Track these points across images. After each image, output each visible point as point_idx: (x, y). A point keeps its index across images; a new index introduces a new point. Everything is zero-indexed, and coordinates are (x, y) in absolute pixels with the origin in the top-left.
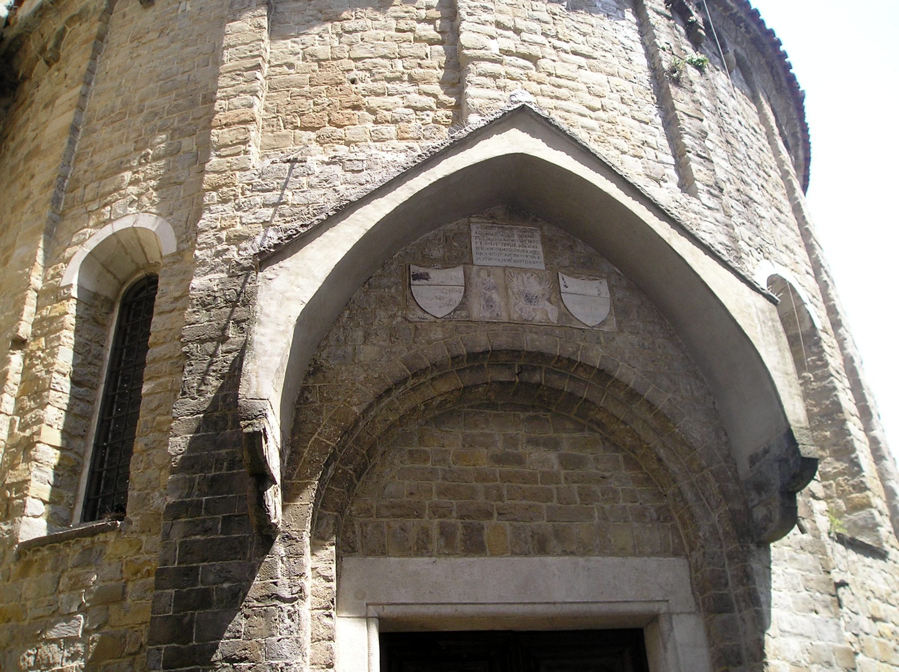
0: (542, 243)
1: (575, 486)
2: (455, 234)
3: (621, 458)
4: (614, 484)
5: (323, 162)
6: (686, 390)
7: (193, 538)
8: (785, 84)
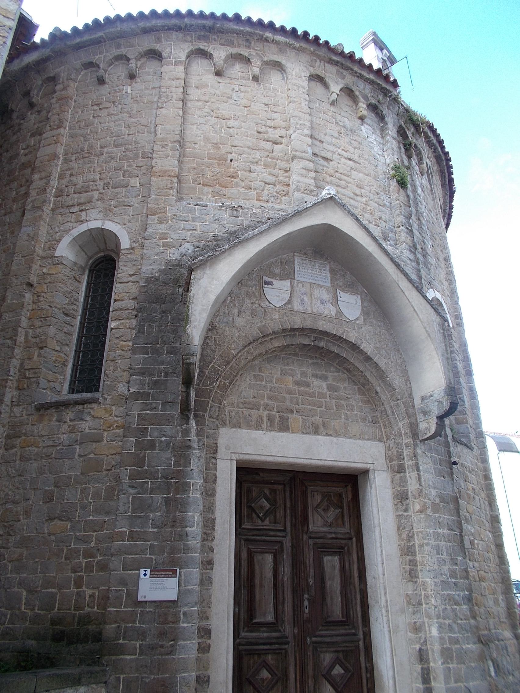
0: (330, 272)
1: (334, 401)
2: (287, 261)
3: (356, 389)
4: (352, 402)
7: (145, 412)
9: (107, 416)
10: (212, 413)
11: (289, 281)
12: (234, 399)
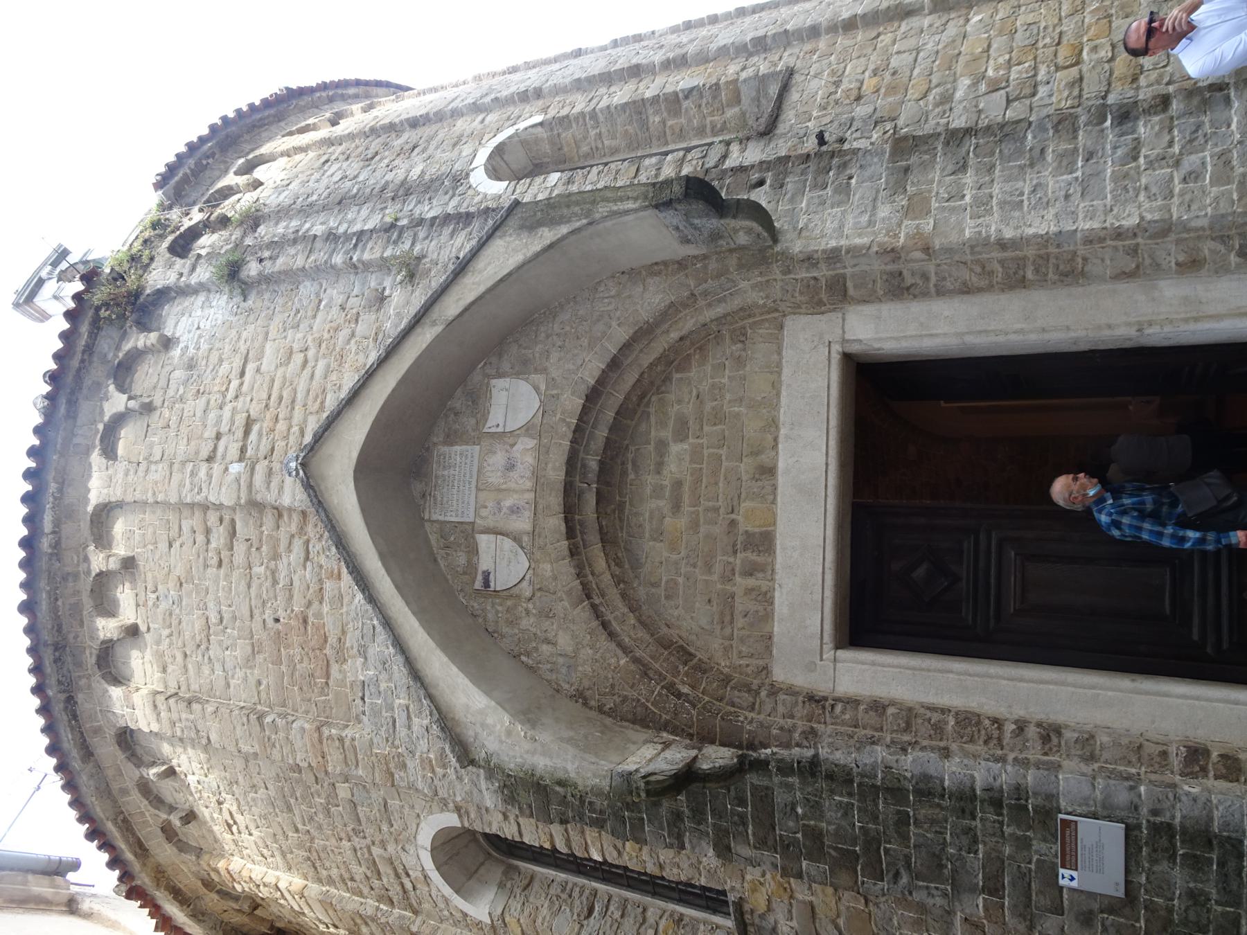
1: (706, 428)
4: (705, 387)
5: (364, 664)
6: (610, 303)
8: (272, 111)
9: (764, 890)
10: (745, 704)
11: (477, 536)
12: (716, 644)
